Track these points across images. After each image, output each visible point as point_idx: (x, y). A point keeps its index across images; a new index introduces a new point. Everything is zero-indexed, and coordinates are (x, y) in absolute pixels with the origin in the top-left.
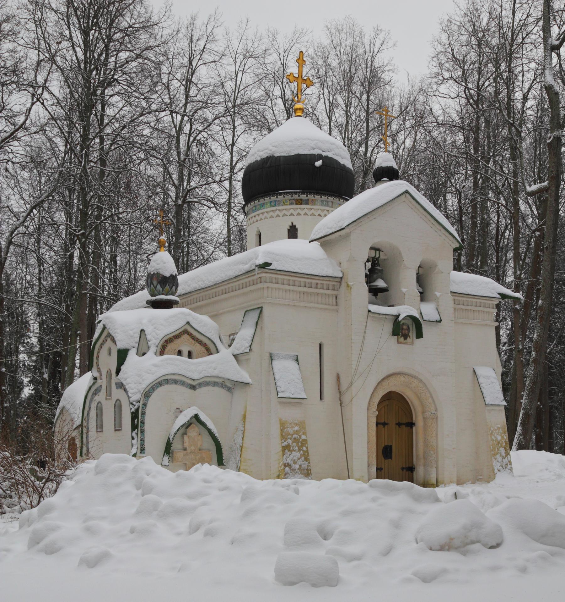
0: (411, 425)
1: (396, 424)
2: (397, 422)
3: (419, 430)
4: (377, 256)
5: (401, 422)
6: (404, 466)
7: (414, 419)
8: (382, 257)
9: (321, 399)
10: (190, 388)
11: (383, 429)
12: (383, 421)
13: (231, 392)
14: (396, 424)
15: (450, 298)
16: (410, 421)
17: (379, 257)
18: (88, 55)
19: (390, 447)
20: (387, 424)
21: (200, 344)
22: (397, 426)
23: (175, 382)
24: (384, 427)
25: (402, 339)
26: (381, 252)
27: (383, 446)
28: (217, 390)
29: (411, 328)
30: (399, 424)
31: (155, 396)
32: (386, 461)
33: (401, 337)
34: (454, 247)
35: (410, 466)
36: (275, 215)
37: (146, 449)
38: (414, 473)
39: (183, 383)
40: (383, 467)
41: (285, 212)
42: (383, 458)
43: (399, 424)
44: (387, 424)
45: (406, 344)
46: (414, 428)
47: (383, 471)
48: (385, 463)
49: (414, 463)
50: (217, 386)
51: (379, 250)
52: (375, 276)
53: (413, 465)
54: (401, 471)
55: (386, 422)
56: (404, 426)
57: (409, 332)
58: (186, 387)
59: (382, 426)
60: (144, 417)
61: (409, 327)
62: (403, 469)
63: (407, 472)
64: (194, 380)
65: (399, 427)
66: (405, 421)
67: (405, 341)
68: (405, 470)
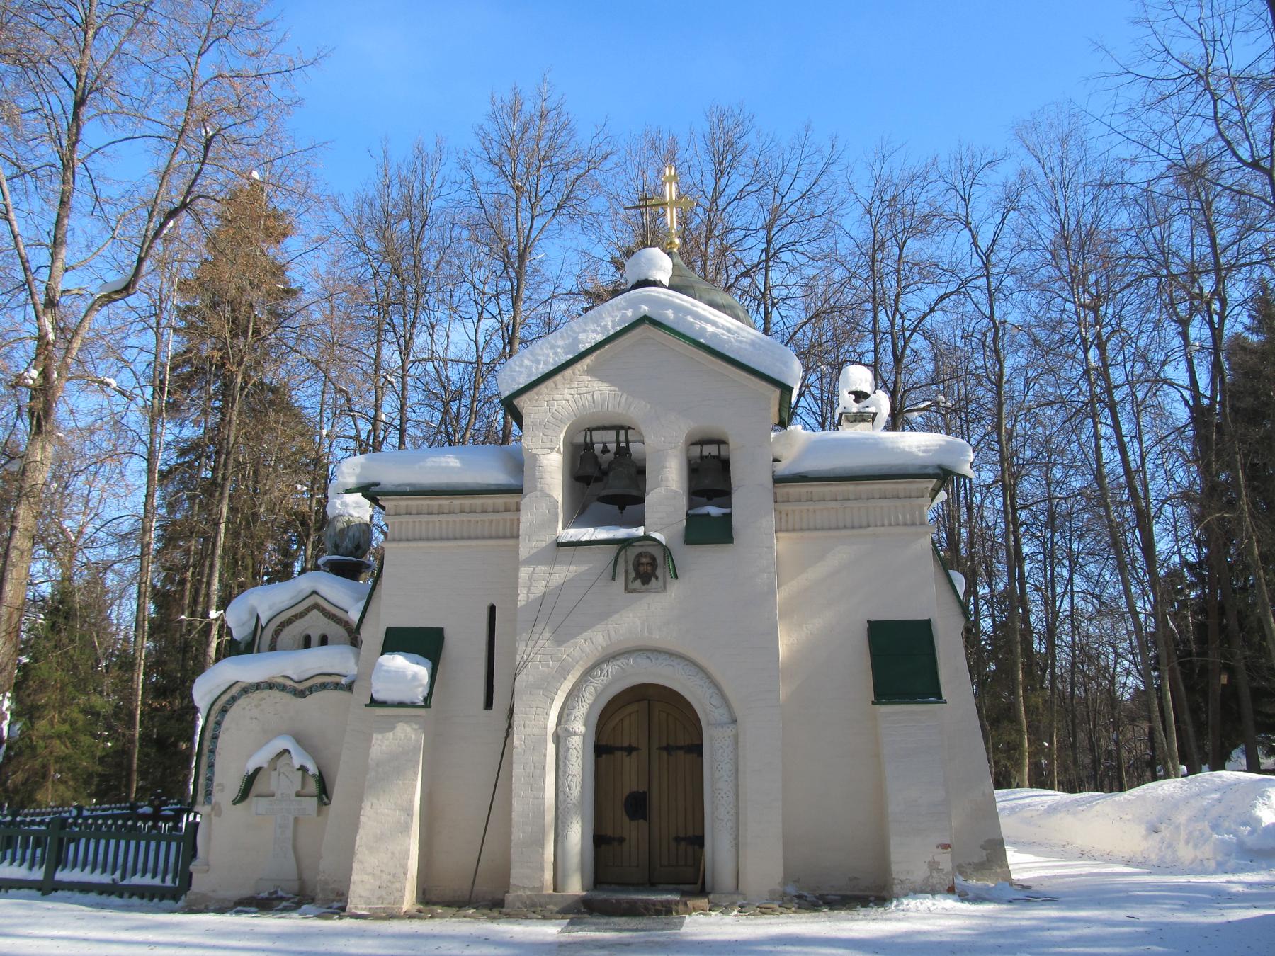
2: (664, 744)
6: (682, 835)
10: (295, 694)
11: (626, 760)
12: (626, 744)
18: (1012, 538)
20: (637, 749)
22: (664, 754)
23: (324, 686)
24: (630, 754)
25: (638, 584)
26: (630, 432)
27: (626, 792)
28: (276, 694)
31: (234, 711)
32: (635, 823)
33: (635, 579)
39: (283, 688)
42: (626, 820)
43: (668, 749)
44: (637, 749)
45: (648, 591)
48: (632, 831)
55: (634, 745)
59: (625, 754)
65: (669, 754)
68: (683, 844)
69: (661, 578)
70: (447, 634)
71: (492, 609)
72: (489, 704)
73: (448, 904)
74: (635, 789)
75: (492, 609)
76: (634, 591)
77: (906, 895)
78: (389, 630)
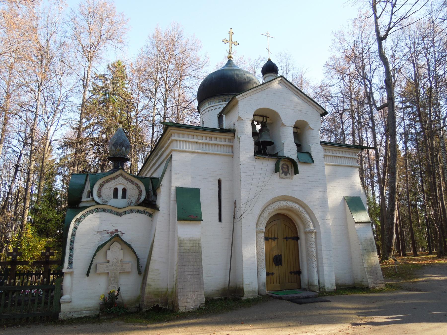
0: (297, 238)
1: (284, 238)
2: (285, 237)
3: (302, 242)
4: (265, 121)
5: (288, 236)
6: (292, 271)
7: (298, 234)
8: (268, 121)
9: (220, 220)
13: (152, 217)
14: (284, 238)
15: (321, 148)
16: (296, 236)
17: (266, 121)
19: (281, 256)
21: (132, 183)
22: (285, 240)
24: (274, 240)
25: (283, 175)
27: (274, 255)
29: (290, 167)
30: (286, 238)
32: (277, 267)
33: (282, 173)
34: (321, 113)
35: (297, 270)
36: (210, 109)
37: (74, 263)
38: (301, 275)
40: (274, 272)
41: (216, 107)
42: (274, 265)
43: (286, 238)
46: (299, 241)
47: (275, 275)
48: (275, 269)
49: (301, 268)
50: (140, 213)
51: (266, 117)
52: (263, 133)
53: (300, 269)
54: (290, 274)
55: (276, 237)
56: (290, 240)
57: (288, 170)
58: (113, 214)
60: (74, 237)
61: (288, 166)
62: (291, 273)
63: (295, 275)
64: (119, 208)
66: (291, 235)
67: (286, 177)
68: (293, 274)
69: (291, 174)
70: (201, 192)
71: (220, 181)
72: (220, 220)
73: (192, 312)
74: (277, 254)
75: (220, 181)
76: (282, 178)
77: (395, 166)
78: (199, 189)
